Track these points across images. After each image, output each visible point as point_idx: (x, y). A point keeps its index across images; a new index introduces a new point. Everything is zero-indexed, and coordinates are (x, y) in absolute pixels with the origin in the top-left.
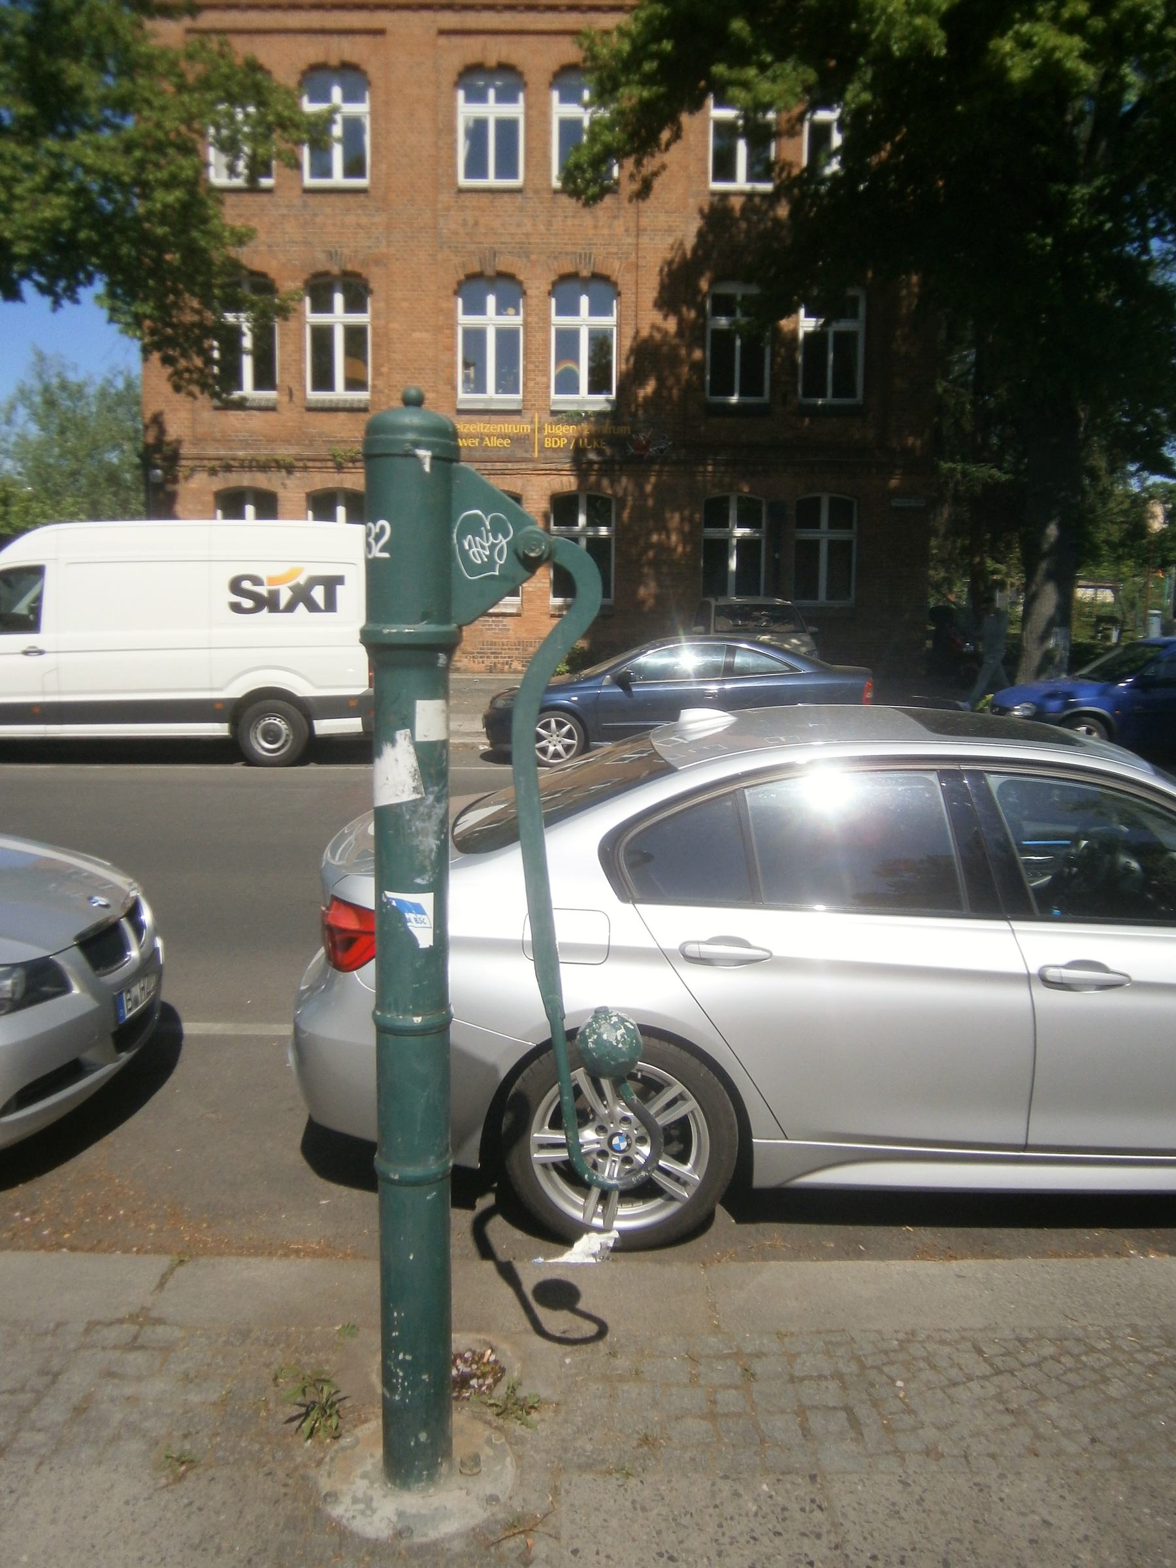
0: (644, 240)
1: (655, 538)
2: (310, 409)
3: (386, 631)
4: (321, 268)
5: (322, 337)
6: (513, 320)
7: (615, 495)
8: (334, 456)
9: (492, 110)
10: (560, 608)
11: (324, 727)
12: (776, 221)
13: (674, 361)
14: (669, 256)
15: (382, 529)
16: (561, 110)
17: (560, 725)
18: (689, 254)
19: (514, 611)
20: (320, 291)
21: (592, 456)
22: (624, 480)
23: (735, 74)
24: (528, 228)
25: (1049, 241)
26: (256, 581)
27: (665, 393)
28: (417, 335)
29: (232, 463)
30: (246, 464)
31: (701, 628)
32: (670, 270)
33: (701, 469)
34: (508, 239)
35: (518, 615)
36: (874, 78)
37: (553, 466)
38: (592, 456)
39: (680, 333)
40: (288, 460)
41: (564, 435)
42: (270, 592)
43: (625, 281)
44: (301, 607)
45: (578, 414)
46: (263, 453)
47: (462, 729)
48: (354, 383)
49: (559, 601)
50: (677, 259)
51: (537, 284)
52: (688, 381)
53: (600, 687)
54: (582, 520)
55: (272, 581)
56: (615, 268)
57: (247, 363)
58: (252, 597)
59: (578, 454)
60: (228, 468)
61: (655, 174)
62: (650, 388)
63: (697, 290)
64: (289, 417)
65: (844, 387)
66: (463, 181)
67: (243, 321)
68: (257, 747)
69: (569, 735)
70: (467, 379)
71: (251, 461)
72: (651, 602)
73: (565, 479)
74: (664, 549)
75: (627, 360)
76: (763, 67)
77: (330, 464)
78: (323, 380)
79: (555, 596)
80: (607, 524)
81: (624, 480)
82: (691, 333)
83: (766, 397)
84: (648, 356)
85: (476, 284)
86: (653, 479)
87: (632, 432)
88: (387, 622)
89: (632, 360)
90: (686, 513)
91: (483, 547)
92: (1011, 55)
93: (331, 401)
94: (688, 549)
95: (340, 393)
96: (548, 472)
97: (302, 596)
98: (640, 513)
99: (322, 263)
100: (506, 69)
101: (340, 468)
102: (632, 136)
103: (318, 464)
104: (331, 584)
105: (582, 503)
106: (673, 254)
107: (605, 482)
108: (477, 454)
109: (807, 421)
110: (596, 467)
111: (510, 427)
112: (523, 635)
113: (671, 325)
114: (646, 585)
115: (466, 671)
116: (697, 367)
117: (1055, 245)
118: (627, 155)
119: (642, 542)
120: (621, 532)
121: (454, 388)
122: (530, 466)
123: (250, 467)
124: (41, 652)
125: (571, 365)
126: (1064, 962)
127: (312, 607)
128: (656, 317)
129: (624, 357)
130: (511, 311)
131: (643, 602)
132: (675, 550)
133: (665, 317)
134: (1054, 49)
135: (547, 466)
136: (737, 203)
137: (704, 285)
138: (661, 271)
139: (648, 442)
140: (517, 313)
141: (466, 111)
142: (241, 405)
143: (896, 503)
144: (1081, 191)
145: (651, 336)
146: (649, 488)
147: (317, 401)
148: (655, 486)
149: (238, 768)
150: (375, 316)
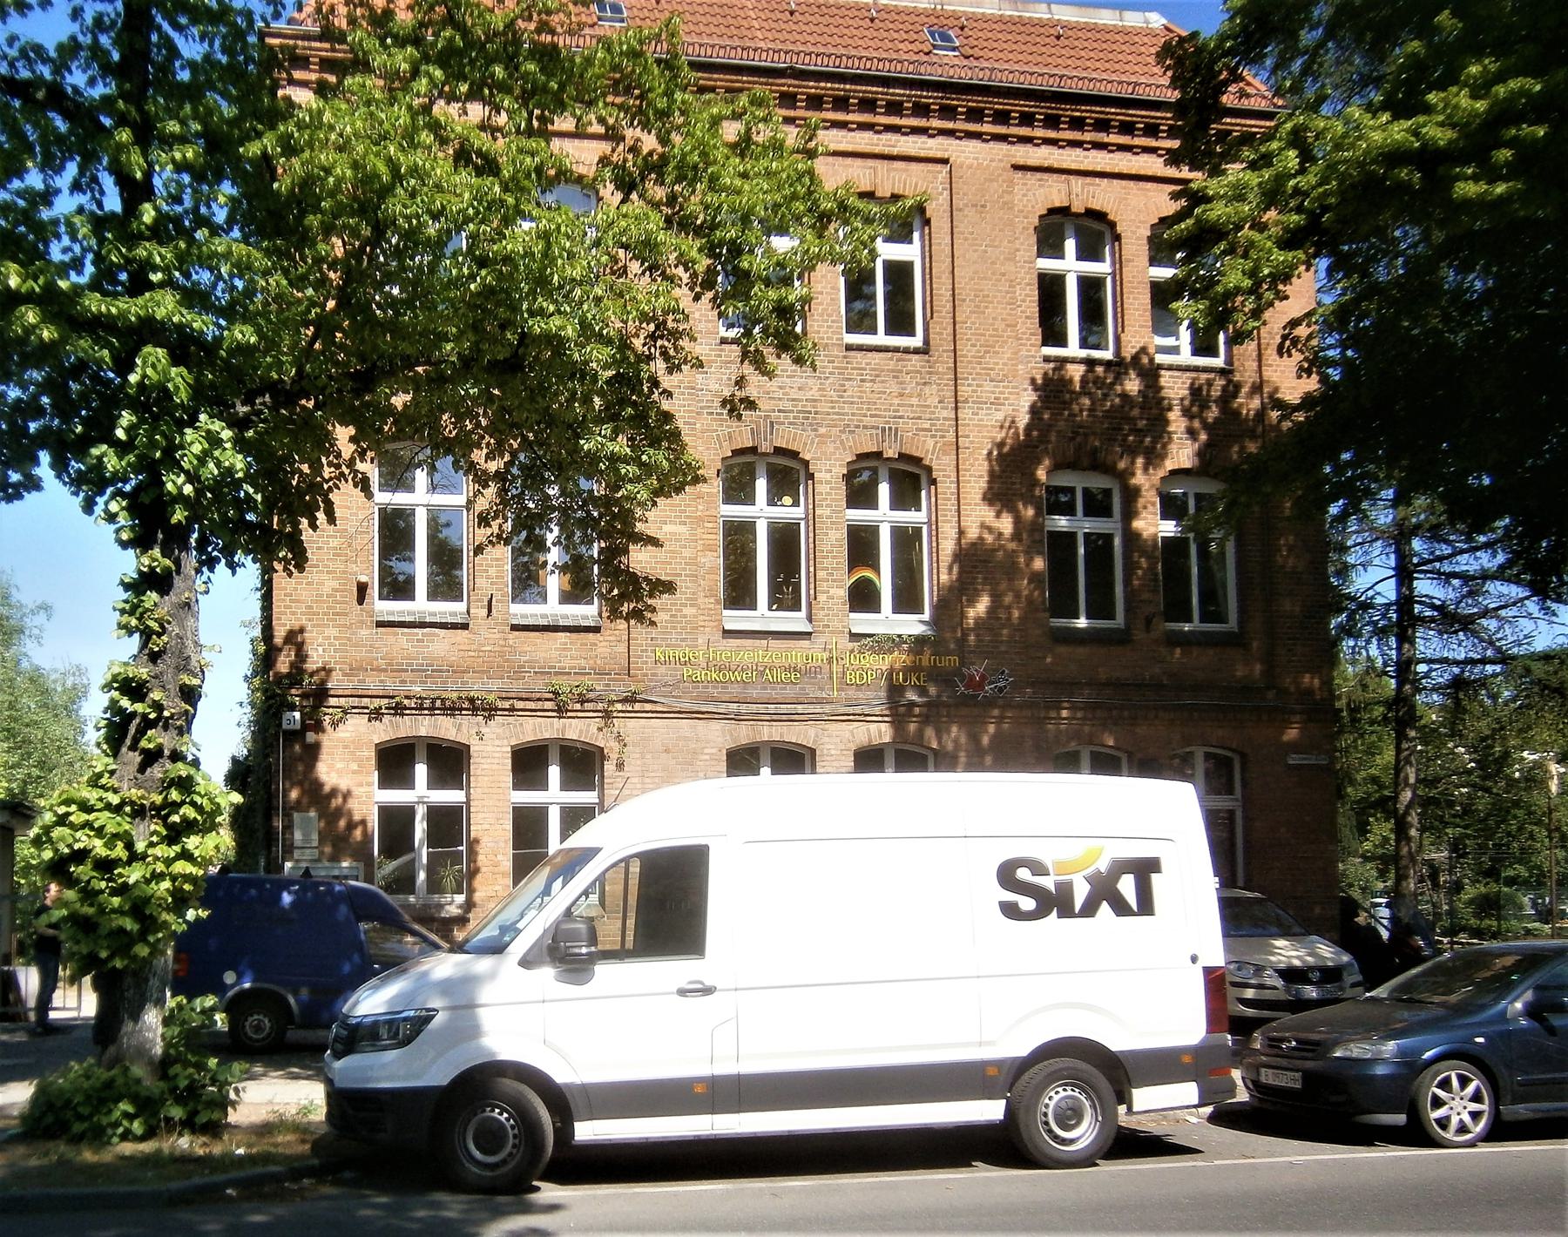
2: (515, 628)
6: (787, 511)
8: (556, 693)
12: (1125, 396)
13: (1011, 569)
14: (999, 437)
17: (1464, 1081)
21: (912, 696)
22: (954, 729)
24: (814, 393)
26: (1038, 868)
29: (406, 702)
30: (427, 703)
33: (1053, 714)
34: (789, 406)
37: (858, 710)
38: (912, 696)
39: (1016, 536)
42: (1058, 885)
43: (942, 466)
44: (1105, 908)
45: (889, 638)
50: (1009, 441)
55: (1062, 867)
58: (1034, 895)
59: (895, 691)
60: (399, 710)
62: (982, 606)
63: (1035, 482)
64: (487, 635)
65: (1212, 608)
69: (1477, 1098)
75: (950, 569)
77: (549, 705)
82: (1027, 533)
83: (1120, 620)
84: (975, 562)
86: (992, 728)
87: (962, 664)
89: (955, 569)
96: (848, 718)
97: (1104, 892)
101: (561, 711)
103: (531, 705)
104: (1144, 869)
106: (1003, 434)
107: (930, 732)
108: (754, 693)
109: (1178, 651)
110: (917, 710)
111: (797, 653)
113: (1006, 525)
116: (1035, 577)
122: (828, 708)
124: (708, 991)
125: (869, 574)
127: (1121, 908)
128: (987, 514)
129: (944, 565)
130: (787, 500)
133: (998, 516)
136: (1076, 372)
138: (990, 453)
139: (983, 677)
140: (796, 504)
143: (1294, 759)
145: (981, 538)
146: (985, 740)
148: (994, 738)
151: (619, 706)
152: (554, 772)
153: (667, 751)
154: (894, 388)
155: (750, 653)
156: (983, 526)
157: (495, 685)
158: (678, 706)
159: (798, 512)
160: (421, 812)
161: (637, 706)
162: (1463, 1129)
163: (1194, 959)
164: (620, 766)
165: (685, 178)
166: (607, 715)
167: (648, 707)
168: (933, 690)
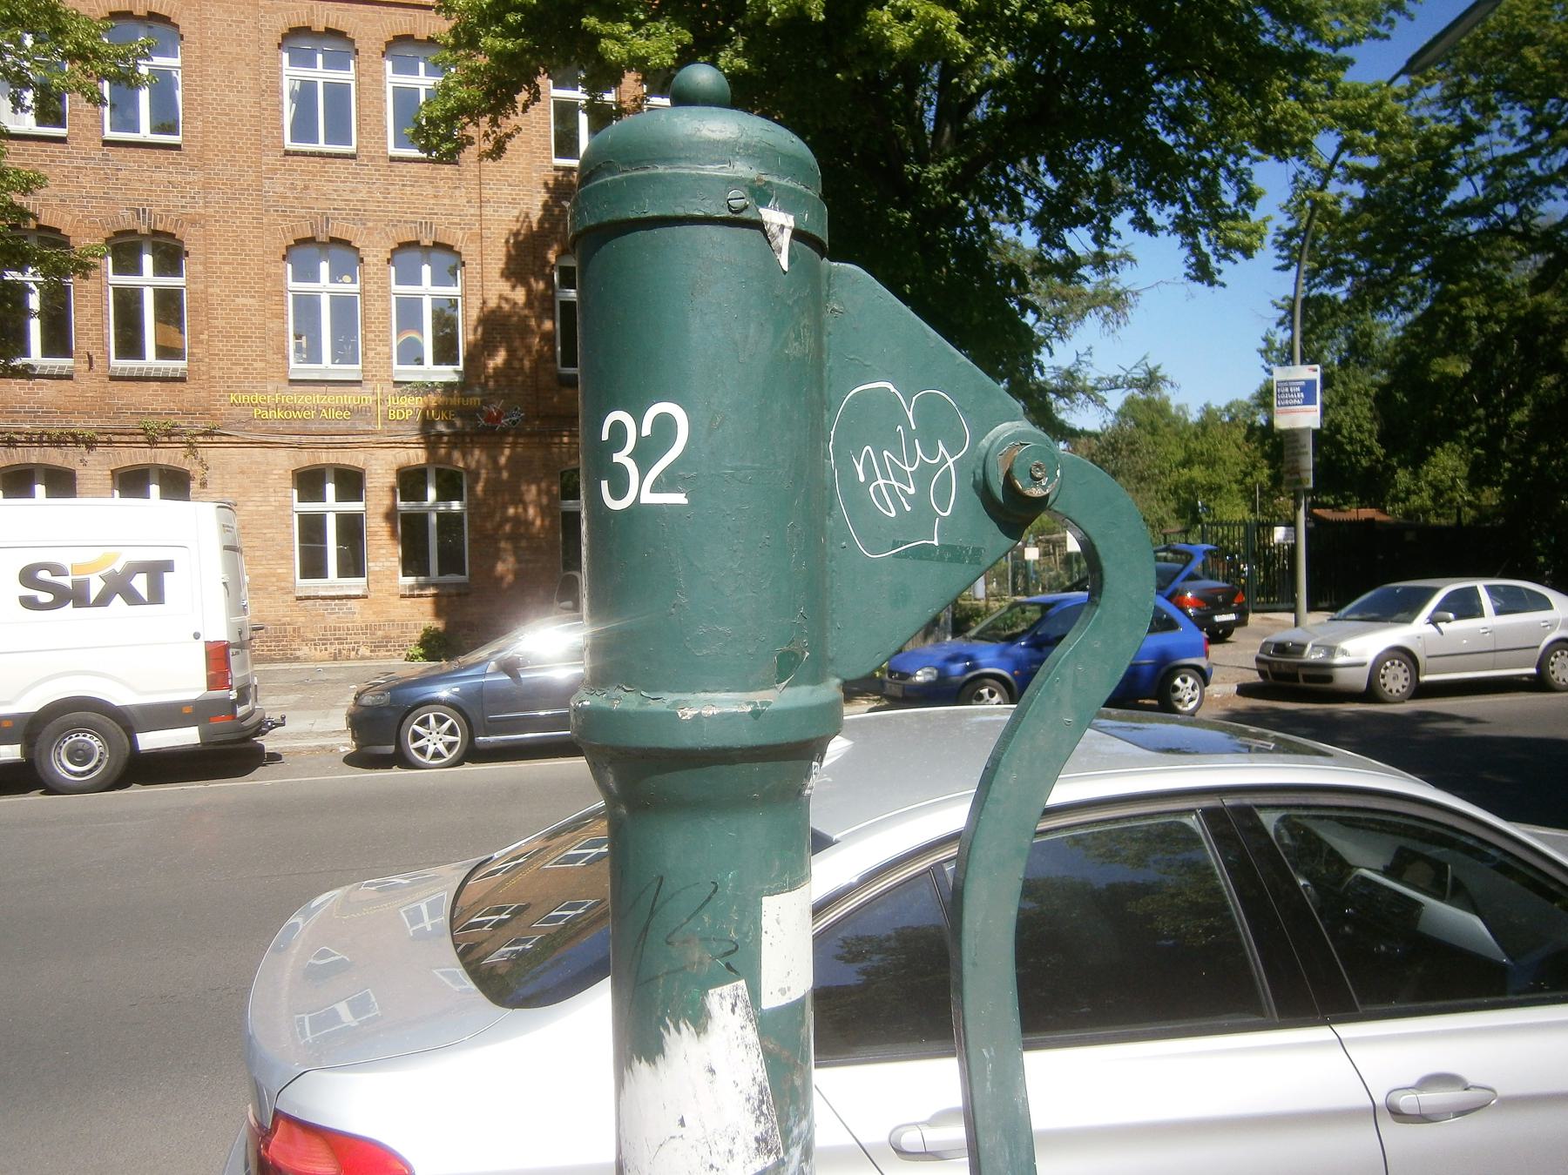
0: (488, 211)
1: (511, 511)
2: (113, 378)
3: (688, 714)
4: (125, 226)
5: (128, 304)
6: (348, 287)
7: (467, 469)
9: (320, 74)
10: (412, 588)
11: (148, 741)
13: (525, 331)
14: (515, 228)
15: (665, 426)
16: (393, 80)
18: (535, 226)
19: (359, 592)
20: (125, 250)
22: (477, 452)
23: (606, 28)
24: (363, 195)
25: (908, 215)
26: (57, 570)
27: (516, 364)
28: (240, 301)
31: (569, 604)
32: (516, 243)
33: (556, 440)
34: (342, 205)
35: (365, 597)
36: (745, 47)
37: (398, 439)
38: (441, 428)
39: (529, 303)
40: (88, 433)
41: (413, 404)
43: (469, 251)
45: (424, 385)
46: (56, 427)
47: (315, 728)
48: (164, 352)
49: (411, 580)
51: (375, 253)
52: (540, 352)
53: (484, 675)
54: (432, 493)
56: (457, 238)
57: (35, 326)
58: (48, 589)
59: (426, 424)
61: (509, 136)
62: (500, 358)
63: (546, 262)
64: (88, 386)
66: (289, 145)
67: (31, 277)
68: (61, 771)
70: (298, 349)
71: (42, 435)
72: (510, 578)
73: (411, 451)
74: (518, 521)
75: (475, 330)
76: (637, 24)
77: (140, 438)
78: (130, 345)
79: (405, 575)
80: (460, 499)
81: (477, 452)
82: (542, 304)
84: (495, 325)
85: (308, 248)
86: (507, 452)
88: (692, 688)
89: (480, 330)
90: (543, 485)
91: (901, 476)
92: (889, 26)
93: (141, 369)
94: (547, 523)
95: (151, 361)
96: (392, 445)
97: (118, 587)
98: (494, 487)
99: (127, 221)
100: (333, 34)
101: (152, 442)
102: (489, 94)
103: (126, 439)
104: (157, 571)
105: (431, 476)
107: (456, 455)
108: (313, 428)
110: (445, 439)
111: (349, 397)
112: (371, 618)
113: (519, 295)
114: (504, 561)
115: (306, 660)
116: (548, 338)
117: (913, 220)
118: (482, 113)
119: (498, 518)
120: (474, 506)
121: (286, 358)
122: (373, 438)
123: (40, 442)
125: (414, 335)
126: (1412, 1081)
127: (132, 598)
128: (504, 287)
129: (471, 328)
130: (347, 278)
131: (502, 578)
132: (533, 523)
133: (514, 287)
134: (934, 20)
135: (392, 439)
137: (552, 257)
138: (507, 241)
139: (500, 413)
140: (354, 281)
141: (291, 75)
142: (26, 373)
144: (934, 171)
145: (499, 307)
146: (503, 460)
147: (123, 369)
148: (509, 458)
149: (35, 798)
150: (190, 280)
151: (200, 439)
152: (330, 489)
153: (242, 472)
154: (429, 191)
155: (315, 397)
156: (501, 297)
157: (95, 423)
158: (249, 438)
159: (356, 288)
160: (433, 519)
161: (216, 439)
162: (437, 755)
163: (197, 636)
164: (203, 484)
165: (968, 23)
166: (190, 445)
167: (225, 439)
168: (458, 423)
